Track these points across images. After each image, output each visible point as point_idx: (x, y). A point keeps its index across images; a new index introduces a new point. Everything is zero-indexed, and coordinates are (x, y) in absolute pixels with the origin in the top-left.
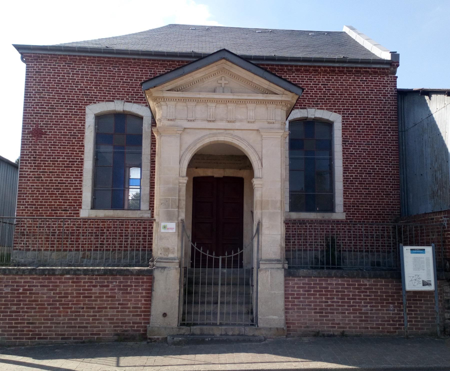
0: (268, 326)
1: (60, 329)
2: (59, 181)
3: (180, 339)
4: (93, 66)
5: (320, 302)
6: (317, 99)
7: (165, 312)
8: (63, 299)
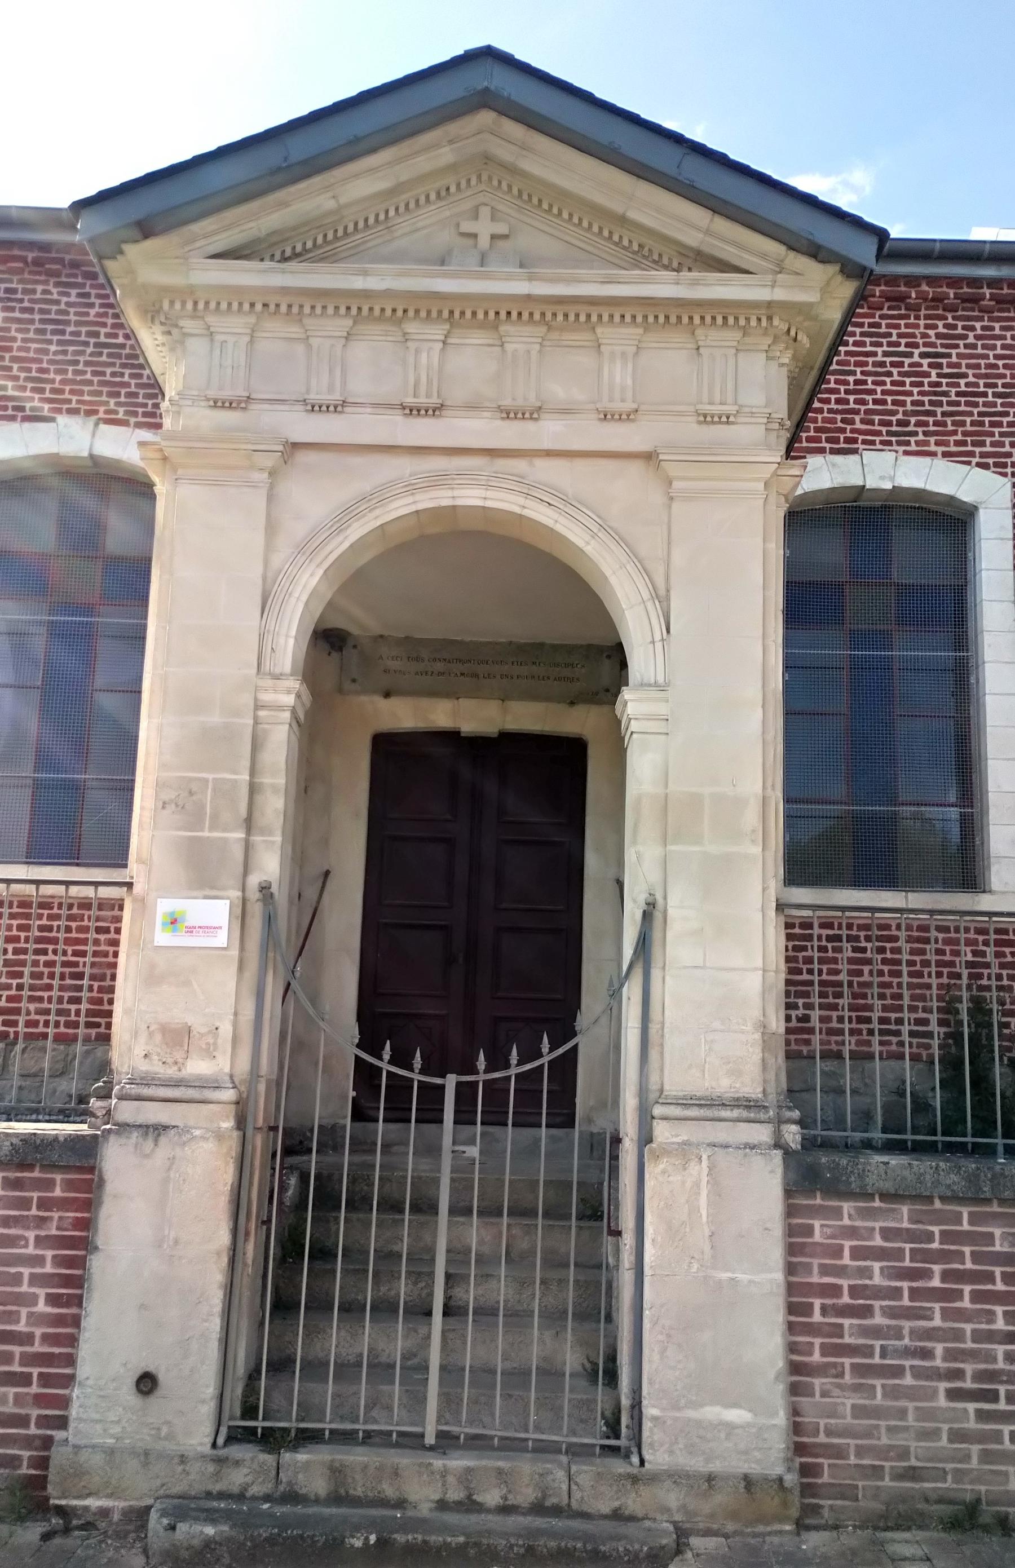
0: (697, 1464)
3: (210, 1531)
5: (978, 1336)
6: (905, 413)
7: (151, 1369)
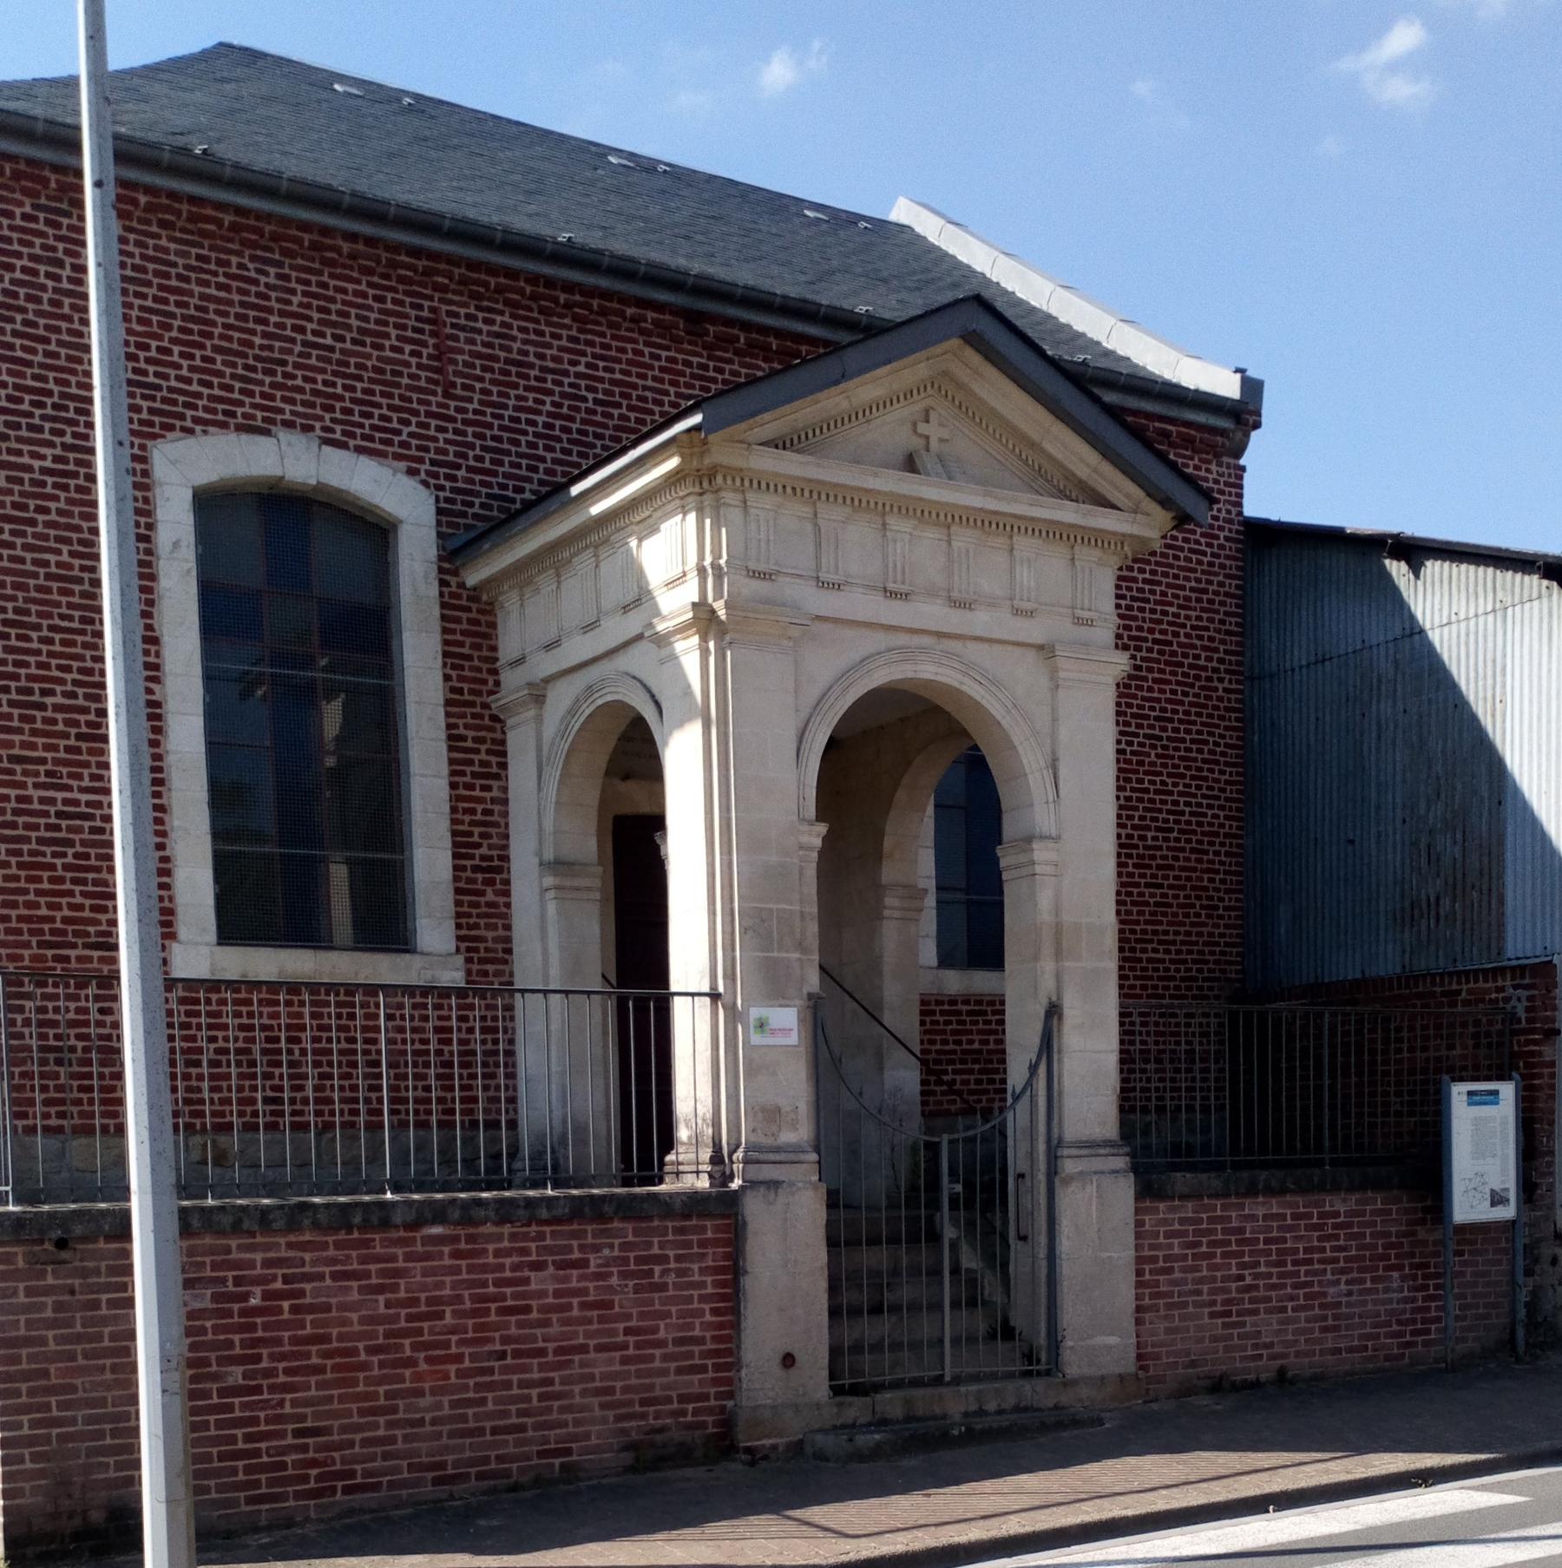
1: (424, 1446)
2: (60, 807)
4: (164, 242)
8: (425, 1325)
